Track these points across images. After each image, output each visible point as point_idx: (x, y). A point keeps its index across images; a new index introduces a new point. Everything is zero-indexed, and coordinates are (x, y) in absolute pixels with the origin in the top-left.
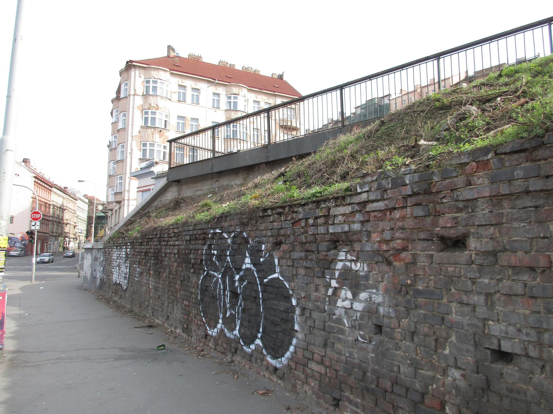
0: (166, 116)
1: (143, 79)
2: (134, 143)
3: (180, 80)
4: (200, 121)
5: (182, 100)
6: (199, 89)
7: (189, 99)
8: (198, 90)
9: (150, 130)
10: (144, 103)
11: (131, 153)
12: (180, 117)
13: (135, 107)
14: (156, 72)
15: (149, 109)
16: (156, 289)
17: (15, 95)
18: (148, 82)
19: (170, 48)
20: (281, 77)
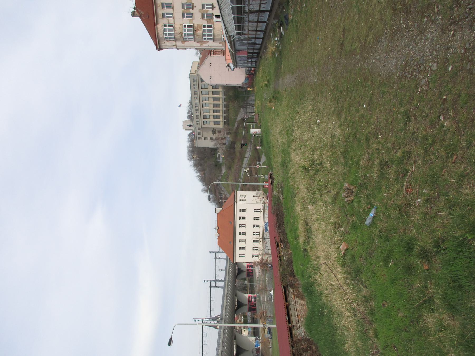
0: (185, 26)
1: (166, 42)
2: (205, 45)
3: (160, 17)
4: (183, 3)
5: (172, 15)
6: (162, 4)
7: (170, 11)
8: (163, 5)
9: (196, 37)
10: (179, 40)
11: (211, 46)
12: (184, 17)
13: (183, 45)
14: (160, 34)
15: (183, 38)
16: (373, 43)
17: (285, 311)
18: (166, 38)
19: (215, 229)
20: (133, 15)
